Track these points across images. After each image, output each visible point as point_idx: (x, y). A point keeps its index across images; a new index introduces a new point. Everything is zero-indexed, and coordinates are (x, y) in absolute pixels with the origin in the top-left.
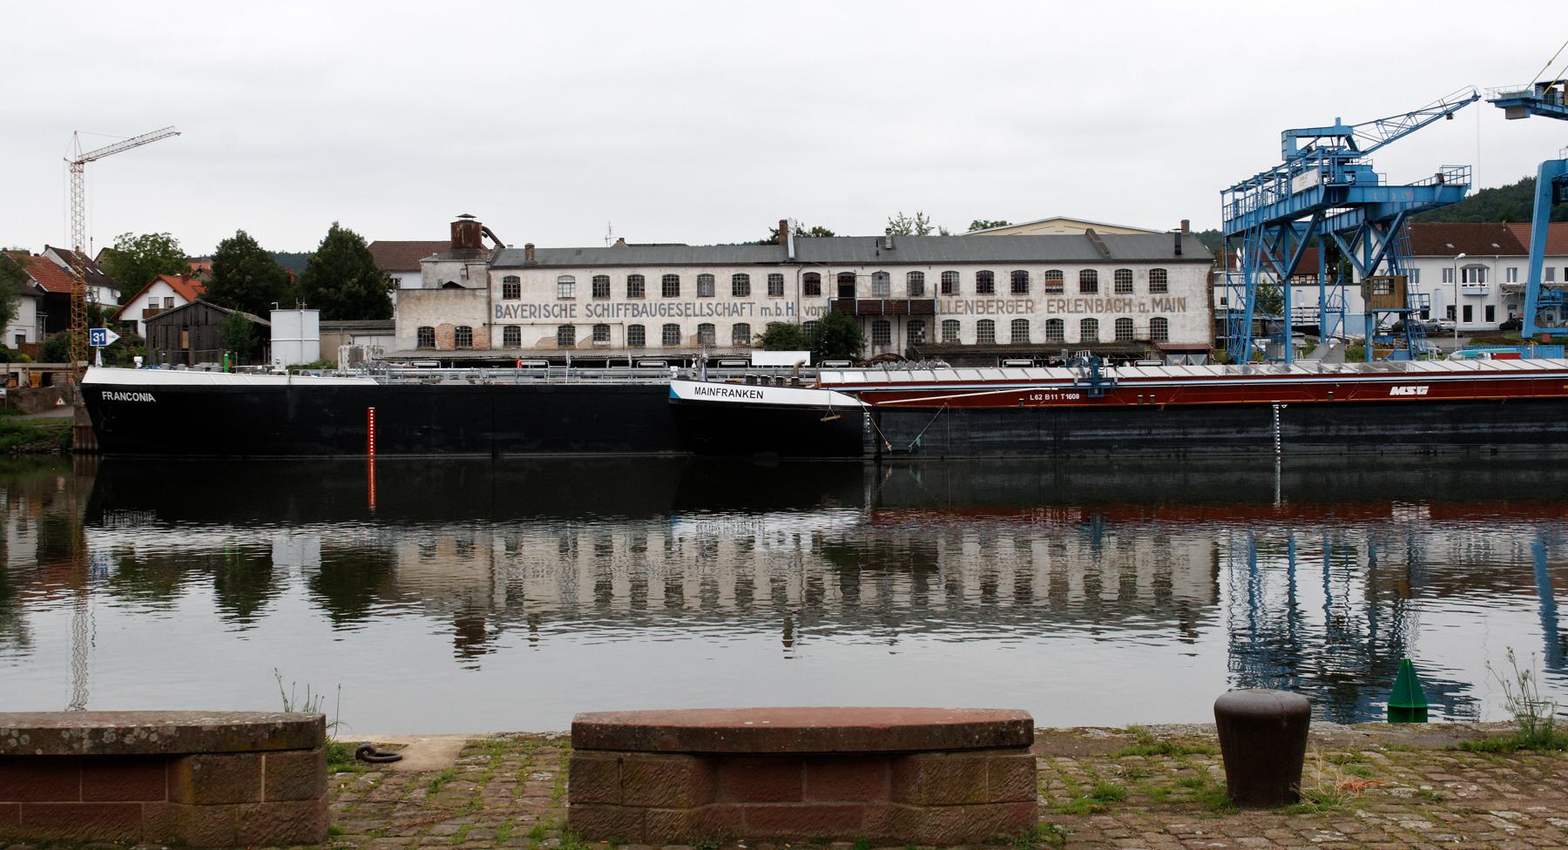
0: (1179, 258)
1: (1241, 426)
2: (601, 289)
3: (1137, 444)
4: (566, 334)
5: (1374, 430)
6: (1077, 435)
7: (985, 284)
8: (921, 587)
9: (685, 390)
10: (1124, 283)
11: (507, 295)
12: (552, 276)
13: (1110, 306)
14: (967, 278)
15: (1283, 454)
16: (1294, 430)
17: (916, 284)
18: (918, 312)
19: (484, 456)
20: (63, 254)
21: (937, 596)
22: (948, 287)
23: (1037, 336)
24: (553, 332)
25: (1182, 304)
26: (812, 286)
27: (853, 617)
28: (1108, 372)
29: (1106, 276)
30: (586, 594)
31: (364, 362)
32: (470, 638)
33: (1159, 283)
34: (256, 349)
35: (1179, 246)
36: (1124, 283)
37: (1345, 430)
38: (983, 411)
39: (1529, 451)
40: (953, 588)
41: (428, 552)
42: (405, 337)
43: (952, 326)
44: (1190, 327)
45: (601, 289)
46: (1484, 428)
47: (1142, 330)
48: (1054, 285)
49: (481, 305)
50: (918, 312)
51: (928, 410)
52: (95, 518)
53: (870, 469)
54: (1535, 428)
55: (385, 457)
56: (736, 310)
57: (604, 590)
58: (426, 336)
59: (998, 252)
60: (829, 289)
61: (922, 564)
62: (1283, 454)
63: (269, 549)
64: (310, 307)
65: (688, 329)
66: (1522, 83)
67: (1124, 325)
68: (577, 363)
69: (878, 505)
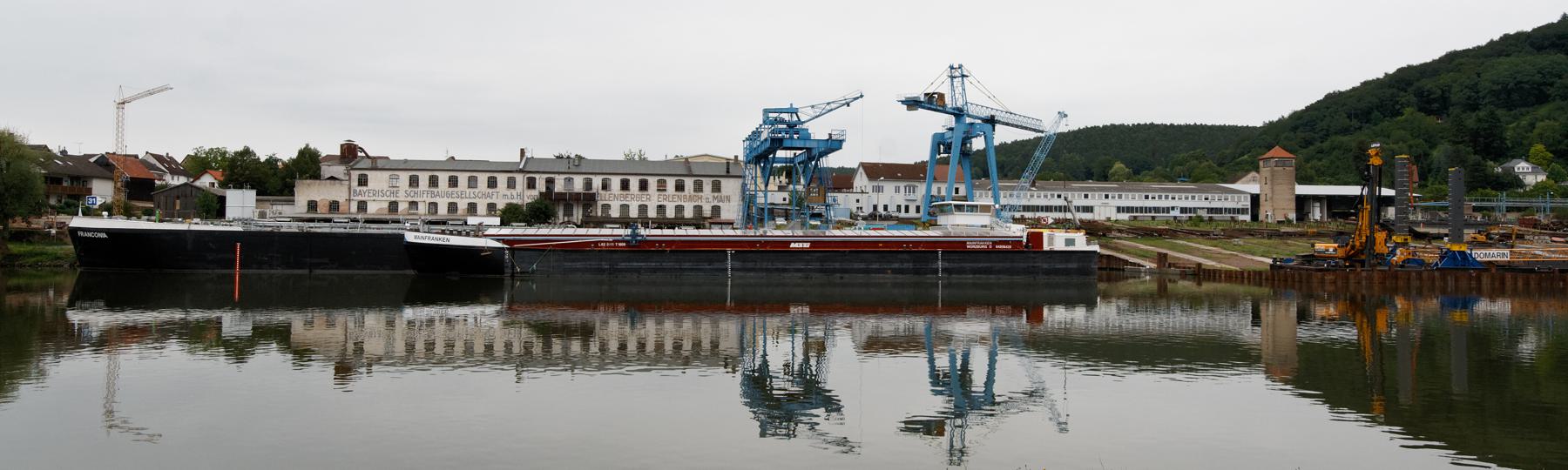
0: (728, 175)
1: (710, 262)
2: (414, 182)
3: (655, 270)
4: (393, 206)
5: (780, 266)
6: (623, 265)
7: (625, 185)
8: (585, 346)
9: (410, 237)
10: (698, 187)
11: (360, 184)
12: (386, 174)
13: (691, 199)
14: (616, 182)
15: (731, 278)
16: (738, 265)
17: (588, 184)
18: (588, 199)
19: (306, 272)
20: (158, 158)
21: (594, 348)
22: (605, 187)
23: (652, 213)
24: (386, 205)
25: (728, 199)
26: (531, 184)
27: (548, 361)
28: (642, 231)
29: (689, 183)
30: (400, 348)
31: (285, 217)
32: (344, 370)
33: (717, 188)
34: (216, 208)
35: (729, 169)
36: (698, 187)
37: (764, 265)
38: (1057, 272)
39: (1005, 278)
40: (603, 348)
41: (309, 324)
42: (300, 206)
43: (606, 207)
44: (732, 210)
45: (414, 182)
46: (837, 265)
47: (707, 212)
48: (662, 187)
49: (345, 189)
50: (588, 199)
51: (542, 250)
52: (71, 305)
53: (508, 281)
54: (862, 266)
55: (245, 271)
56: (488, 196)
57: (410, 347)
58: (312, 206)
59: (637, 172)
60: (541, 186)
61: (586, 332)
62: (731, 278)
63: (289, 325)
64: (252, 188)
65: (462, 205)
66: (918, 92)
67: (698, 209)
68: (367, 221)
69: (511, 303)
